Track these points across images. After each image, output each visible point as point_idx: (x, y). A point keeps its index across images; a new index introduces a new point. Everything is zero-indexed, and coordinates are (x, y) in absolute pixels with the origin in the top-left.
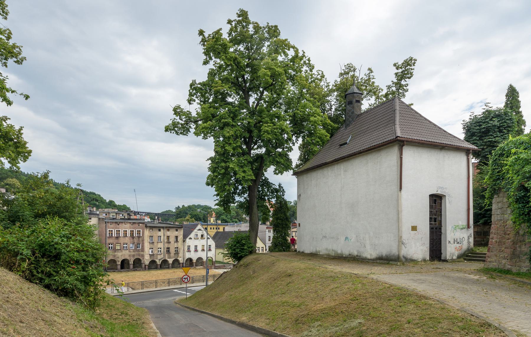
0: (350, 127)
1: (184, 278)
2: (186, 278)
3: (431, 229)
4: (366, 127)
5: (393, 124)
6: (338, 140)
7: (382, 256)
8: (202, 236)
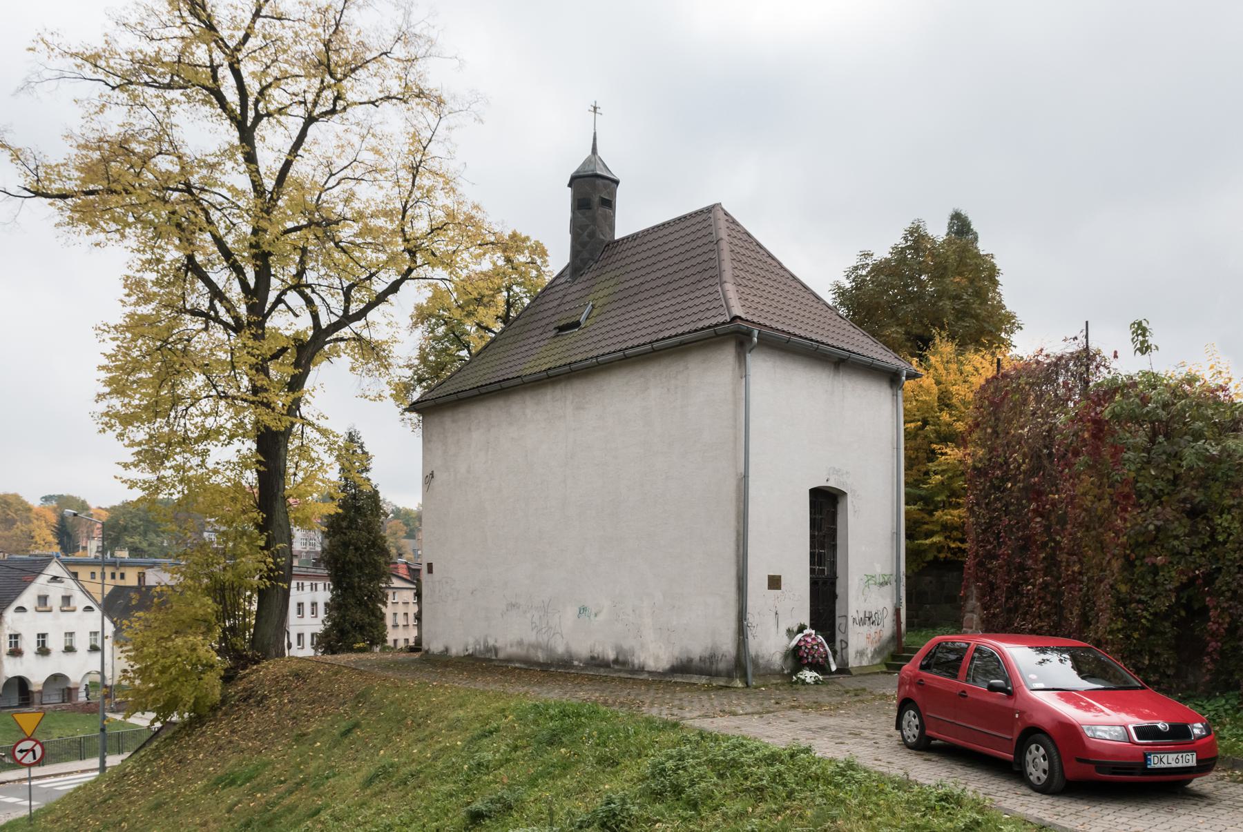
0: (584, 278)
1: (21, 751)
2: (27, 751)
3: (814, 583)
4: (637, 282)
5: (717, 281)
6: (549, 313)
7: (690, 660)
8: (67, 599)
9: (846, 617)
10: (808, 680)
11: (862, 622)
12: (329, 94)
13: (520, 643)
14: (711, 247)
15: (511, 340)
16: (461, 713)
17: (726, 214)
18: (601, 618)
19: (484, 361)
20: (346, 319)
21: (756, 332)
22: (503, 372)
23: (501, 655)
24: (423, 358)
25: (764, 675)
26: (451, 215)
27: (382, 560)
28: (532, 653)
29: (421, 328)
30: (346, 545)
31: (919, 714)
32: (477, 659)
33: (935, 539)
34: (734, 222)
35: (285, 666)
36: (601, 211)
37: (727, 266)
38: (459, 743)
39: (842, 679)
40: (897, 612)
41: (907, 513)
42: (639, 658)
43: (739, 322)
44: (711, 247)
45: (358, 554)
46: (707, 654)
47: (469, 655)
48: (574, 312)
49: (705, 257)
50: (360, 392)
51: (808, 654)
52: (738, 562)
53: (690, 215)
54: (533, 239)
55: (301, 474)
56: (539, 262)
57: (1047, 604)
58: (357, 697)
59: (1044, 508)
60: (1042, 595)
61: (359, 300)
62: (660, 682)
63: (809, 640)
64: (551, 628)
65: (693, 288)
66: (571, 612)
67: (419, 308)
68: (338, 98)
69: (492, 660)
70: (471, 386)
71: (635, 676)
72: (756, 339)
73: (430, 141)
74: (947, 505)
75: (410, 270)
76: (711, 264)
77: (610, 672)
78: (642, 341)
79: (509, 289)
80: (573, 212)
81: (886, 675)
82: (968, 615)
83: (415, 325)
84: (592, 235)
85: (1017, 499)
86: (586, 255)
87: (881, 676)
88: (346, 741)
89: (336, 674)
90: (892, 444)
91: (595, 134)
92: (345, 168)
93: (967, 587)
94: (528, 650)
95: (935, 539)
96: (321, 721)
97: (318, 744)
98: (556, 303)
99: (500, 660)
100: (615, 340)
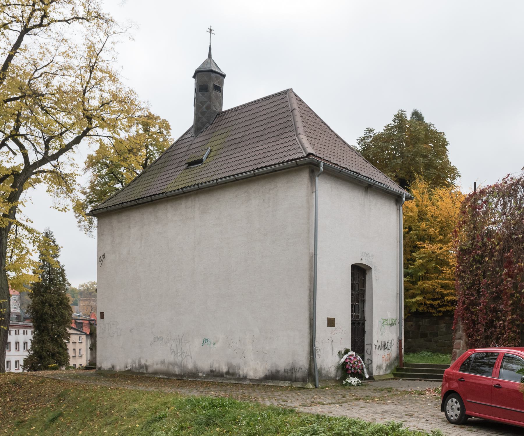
4: (240, 135)
6: (181, 155)
7: (278, 372)
9: (371, 344)
10: (353, 383)
11: (380, 348)
12: (38, 14)
13: (163, 362)
14: (288, 114)
15: (156, 171)
16: (136, 406)
17: (296, 95)
18: (218, 345)
19: (138, 184)
20: (45, 160)
21: (322, 164)
22: (152, 191)
23: (150, 370)
24: (92, 188)
25: (325, 381)
26: (115, 96)
27: (66, 313)
28: (171, 368)
29: (91, 169)
30: (43, 303)
31: (460, 400)
32: (134, 373)
33: (418, 298)
34: (301, 100)
35: (6, 378)
36: (214, 93)
37: (300, 124)
38: (137, 425)
39: (369, 382)
40: (400, 341)
41: (405, 281)
42: (243, 371)
43: (312, 157)
44: (288, 114)
45: (51, 308)
46: (289, 368)
47: (128, 370)
48: (198, 154)
49: (285, 120)
50: (54, 205)
51: (351, 367)
52: (310, 309)
53: (273, 96)
54: (162, 118)
55: (15, 257)
56: (165, 132)
57: (514, 332)
58: (58, 396)
59: (513, 272)
60: (510, 327)
61: (55, 145)
62: (258, 385)
63: (352, 358)
64: (183, 352)
65: (278, 138)
66: (197, 342)
67: (90, 157)
68: (45, 16)
69: (144, 373)
70: (131, 199)
71: (241, 382)
72: (322, 168)
73: (101, 50)
74: (424, 278)
75: (88, 129)
76: (289, 124)
77: (224, 380)
78: (247, 169)
79: (147, 148)
80: (196, 92)
81: (395, 380)
82: (457, 341)
83: (88, 167)
84: (208, 108)
85: (492, 267)
86: (204, 120)
87: (392, 381)
88: (54, 426)
89: (42, 382)
90: (397, 239)
91: (210, 46)
92: (45, 66)
93: (456, 324)
94: (168, 367)
95: (418, 298)
96: (34, 412)
97: (34, 427)
98: (185, 149)
99: (149, 373)
100: (227, 170)
